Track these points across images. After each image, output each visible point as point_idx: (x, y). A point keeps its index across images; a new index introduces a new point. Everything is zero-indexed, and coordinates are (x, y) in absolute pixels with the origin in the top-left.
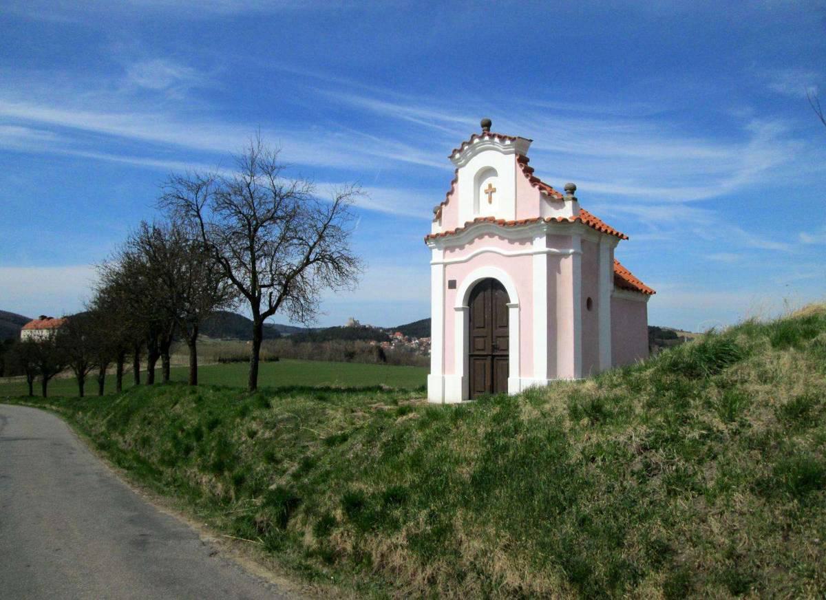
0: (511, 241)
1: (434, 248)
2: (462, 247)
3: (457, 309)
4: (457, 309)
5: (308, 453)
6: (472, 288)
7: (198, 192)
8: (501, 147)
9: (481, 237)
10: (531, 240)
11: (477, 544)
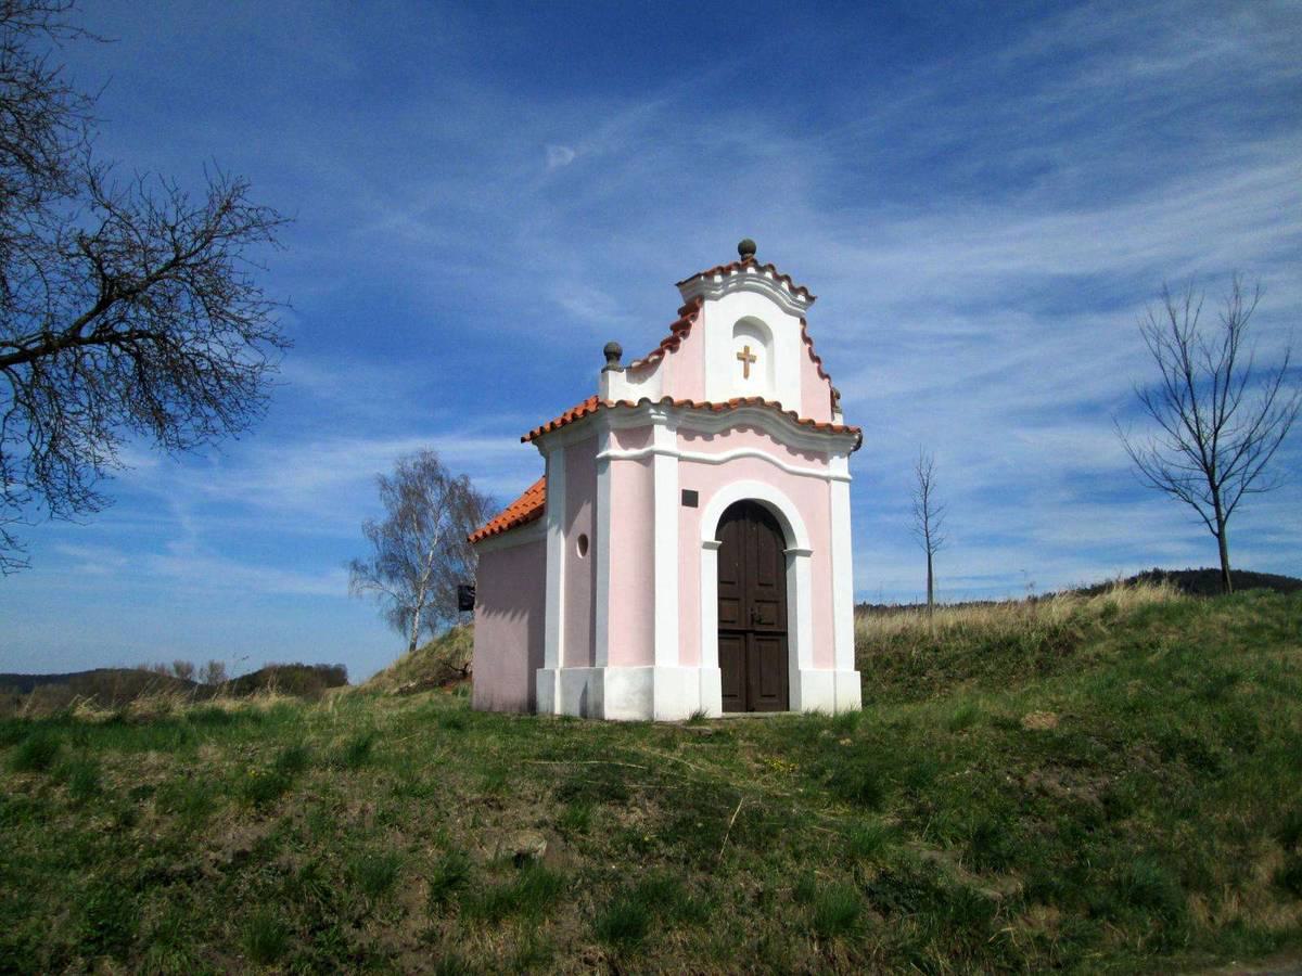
0: (792, 450)
1: (660, 422)
2: (708, 437)
3: (807, 554)
4: (807, 554)
5: (529, 717)
6: (775, 514)
7: (1241, 453)
8: (786, 300)
9: (742, 428)
10: (824, 458)
11: (1053, 823)
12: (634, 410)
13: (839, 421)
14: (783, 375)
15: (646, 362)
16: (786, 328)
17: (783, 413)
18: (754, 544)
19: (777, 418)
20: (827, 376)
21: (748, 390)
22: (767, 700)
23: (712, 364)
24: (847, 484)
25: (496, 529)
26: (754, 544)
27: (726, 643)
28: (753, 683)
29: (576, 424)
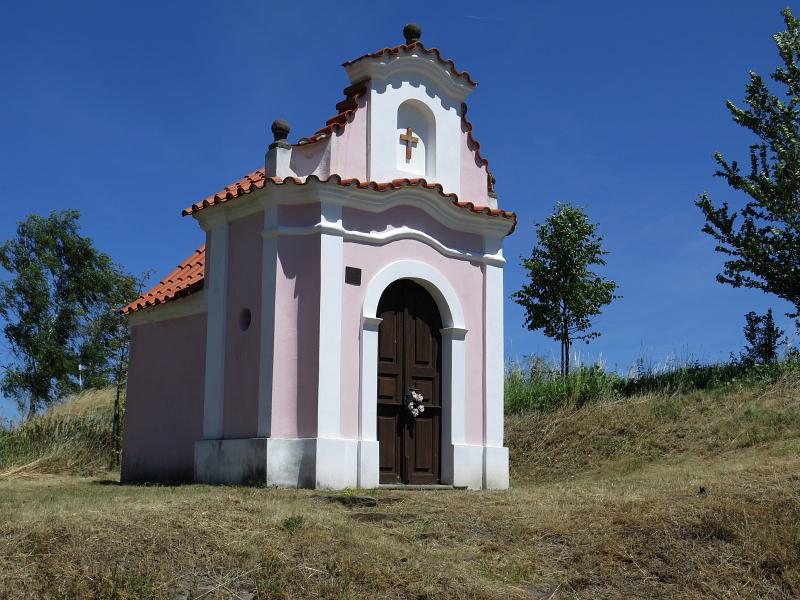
12: (298, 187)
13: (493, 205)
14: (450, 165)
15: (314, 139)
16: (447, 122)
17: (444, 195)
18: (412, 319)
19: (437, 200)
20: (485, 162)
21: (414, 170)
22: (420, 474)
23: (376, 147)
24: (500, 271)
25: (152, 301)
26: (412, 319)
27: (381, 418)
28: (407, 455)
29: (243, 199)
